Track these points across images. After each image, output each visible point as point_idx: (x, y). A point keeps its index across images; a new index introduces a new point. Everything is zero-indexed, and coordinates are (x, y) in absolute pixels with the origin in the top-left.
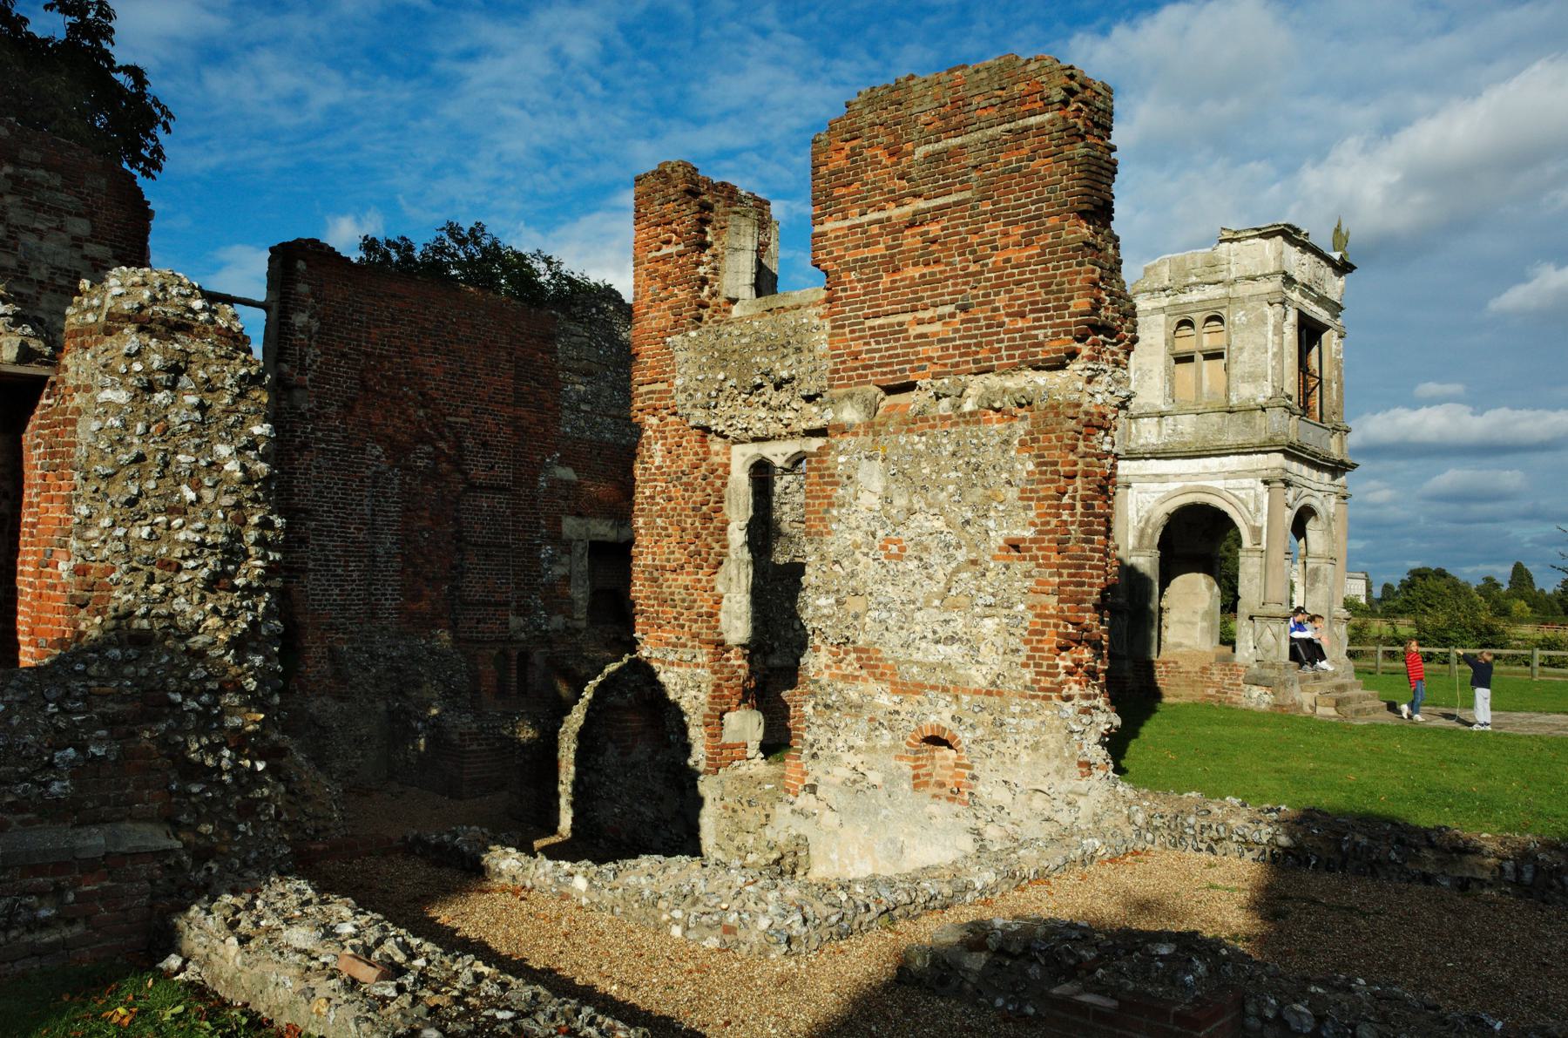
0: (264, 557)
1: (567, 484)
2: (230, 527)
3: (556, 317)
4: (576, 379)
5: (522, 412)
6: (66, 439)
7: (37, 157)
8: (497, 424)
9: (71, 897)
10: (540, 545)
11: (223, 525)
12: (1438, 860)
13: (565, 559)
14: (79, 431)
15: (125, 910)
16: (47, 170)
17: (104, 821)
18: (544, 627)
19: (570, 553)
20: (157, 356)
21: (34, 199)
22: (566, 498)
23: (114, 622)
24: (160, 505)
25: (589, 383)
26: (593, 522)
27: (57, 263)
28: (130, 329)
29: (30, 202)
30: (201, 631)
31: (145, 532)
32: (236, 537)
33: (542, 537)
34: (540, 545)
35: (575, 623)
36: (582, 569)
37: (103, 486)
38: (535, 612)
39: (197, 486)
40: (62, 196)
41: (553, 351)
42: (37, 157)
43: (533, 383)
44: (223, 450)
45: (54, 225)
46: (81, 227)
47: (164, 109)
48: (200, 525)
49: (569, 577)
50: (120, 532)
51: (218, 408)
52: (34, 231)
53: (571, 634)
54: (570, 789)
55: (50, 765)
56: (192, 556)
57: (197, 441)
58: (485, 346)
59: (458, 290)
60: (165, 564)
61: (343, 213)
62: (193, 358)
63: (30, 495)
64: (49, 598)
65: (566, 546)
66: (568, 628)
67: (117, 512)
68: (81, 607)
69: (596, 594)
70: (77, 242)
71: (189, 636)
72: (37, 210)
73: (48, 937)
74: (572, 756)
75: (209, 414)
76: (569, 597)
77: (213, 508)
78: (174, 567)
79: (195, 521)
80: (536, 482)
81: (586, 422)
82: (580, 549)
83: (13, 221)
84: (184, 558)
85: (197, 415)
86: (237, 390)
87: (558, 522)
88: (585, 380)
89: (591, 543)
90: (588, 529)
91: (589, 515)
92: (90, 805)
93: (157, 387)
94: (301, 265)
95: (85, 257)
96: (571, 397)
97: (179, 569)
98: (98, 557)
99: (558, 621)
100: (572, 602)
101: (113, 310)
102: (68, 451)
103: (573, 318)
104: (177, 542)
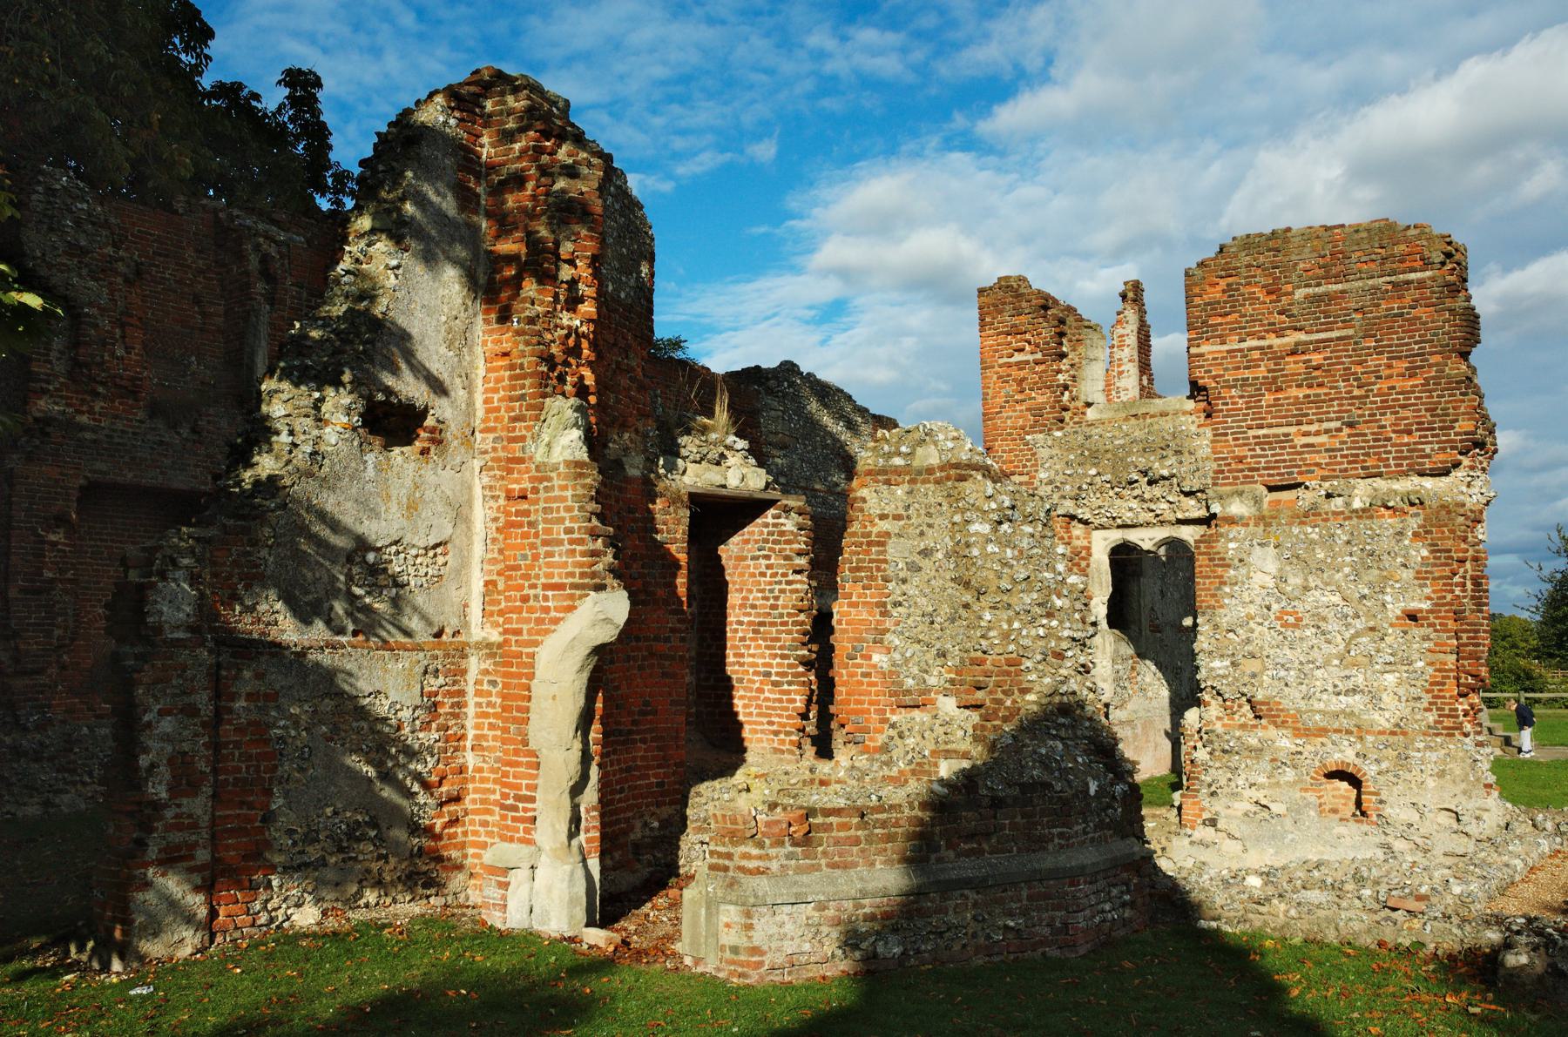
4: (775, 452)
6: (873, 557)
25: (785, 456)
88: (782, 453)
103: (770, 392)
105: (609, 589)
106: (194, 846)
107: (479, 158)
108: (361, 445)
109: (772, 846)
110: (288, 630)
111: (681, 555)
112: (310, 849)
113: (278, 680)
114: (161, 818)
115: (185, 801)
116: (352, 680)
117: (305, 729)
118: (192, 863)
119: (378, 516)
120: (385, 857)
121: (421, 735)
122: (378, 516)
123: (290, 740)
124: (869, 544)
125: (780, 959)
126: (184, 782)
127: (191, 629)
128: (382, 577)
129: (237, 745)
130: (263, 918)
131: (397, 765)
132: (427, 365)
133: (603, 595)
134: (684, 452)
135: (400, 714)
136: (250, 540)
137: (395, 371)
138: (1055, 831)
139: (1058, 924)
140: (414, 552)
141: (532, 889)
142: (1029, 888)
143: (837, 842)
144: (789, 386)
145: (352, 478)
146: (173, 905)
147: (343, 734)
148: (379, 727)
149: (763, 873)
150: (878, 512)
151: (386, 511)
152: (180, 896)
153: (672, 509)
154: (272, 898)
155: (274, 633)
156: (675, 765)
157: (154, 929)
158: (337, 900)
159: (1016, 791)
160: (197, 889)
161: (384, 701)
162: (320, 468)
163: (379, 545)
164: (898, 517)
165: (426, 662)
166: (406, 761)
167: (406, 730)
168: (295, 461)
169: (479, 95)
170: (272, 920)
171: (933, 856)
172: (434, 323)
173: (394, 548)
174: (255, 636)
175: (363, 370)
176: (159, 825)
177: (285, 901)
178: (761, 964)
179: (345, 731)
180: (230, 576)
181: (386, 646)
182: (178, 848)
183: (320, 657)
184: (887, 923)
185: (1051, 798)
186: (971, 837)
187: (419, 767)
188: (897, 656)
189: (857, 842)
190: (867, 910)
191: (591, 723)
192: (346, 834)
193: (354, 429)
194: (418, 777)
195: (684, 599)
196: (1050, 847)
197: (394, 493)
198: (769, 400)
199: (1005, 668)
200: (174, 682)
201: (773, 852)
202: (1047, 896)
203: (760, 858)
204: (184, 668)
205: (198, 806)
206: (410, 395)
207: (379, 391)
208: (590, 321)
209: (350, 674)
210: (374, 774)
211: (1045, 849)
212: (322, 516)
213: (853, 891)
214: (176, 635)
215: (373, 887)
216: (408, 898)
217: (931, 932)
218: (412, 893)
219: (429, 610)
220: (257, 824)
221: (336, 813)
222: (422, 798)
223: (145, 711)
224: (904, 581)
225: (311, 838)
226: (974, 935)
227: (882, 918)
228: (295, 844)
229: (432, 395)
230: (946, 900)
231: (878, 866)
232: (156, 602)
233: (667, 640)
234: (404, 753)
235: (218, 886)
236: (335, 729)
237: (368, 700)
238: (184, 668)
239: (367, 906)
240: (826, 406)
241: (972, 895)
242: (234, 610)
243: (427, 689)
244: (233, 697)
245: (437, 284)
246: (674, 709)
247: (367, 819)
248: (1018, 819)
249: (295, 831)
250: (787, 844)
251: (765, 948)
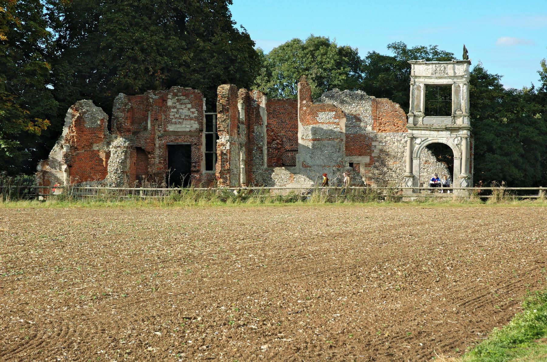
12: (42, 165)
42: (181, 94)
46: (189, 106)
61: (122, 136)
70: (189, 109)
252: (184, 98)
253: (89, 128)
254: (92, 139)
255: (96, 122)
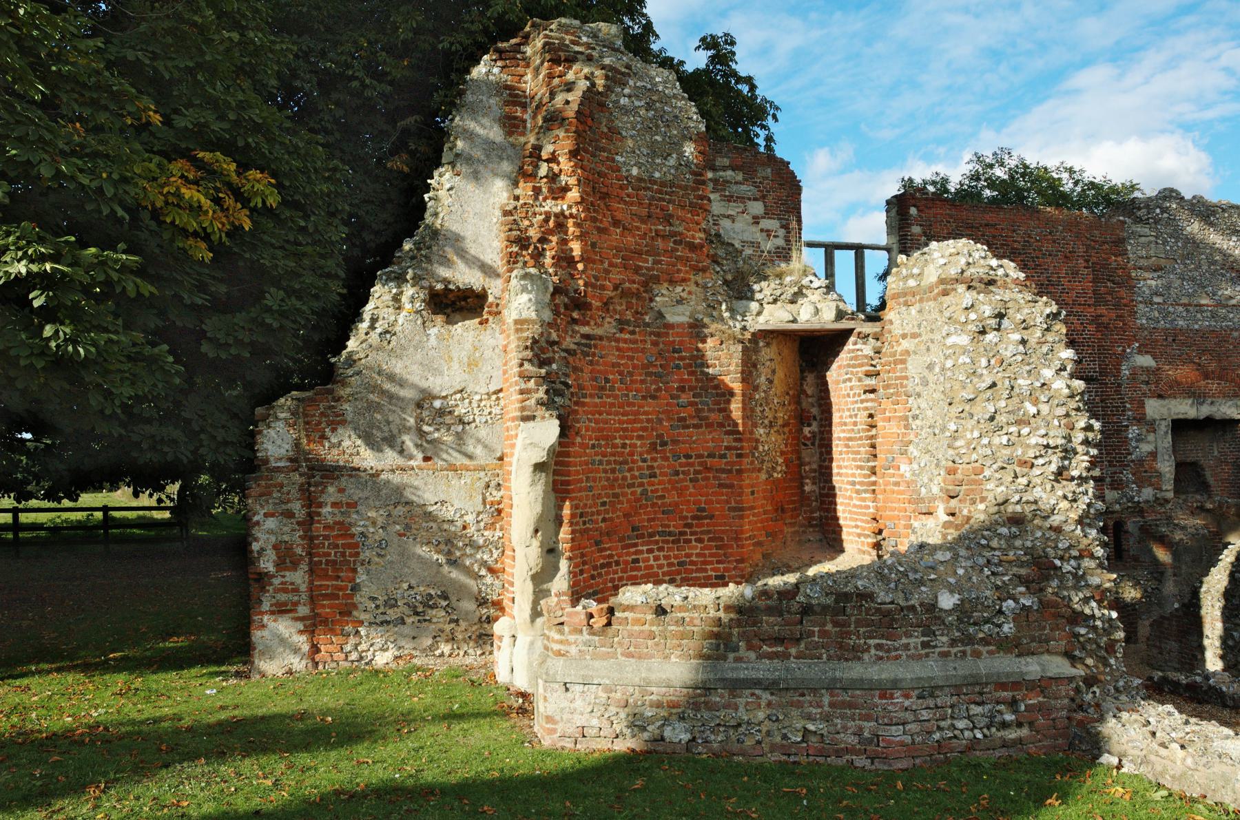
0: (1087, 453)
1: (1147, 370)
2: (1063, 431)
3: (1124, 222)
4: (1147, 275)
5: (1102, 310)
6: (898, 374)
7: (726, 162)
8: (1082, 324)
9: (1023, 708)
10: (1127, 426)
11: (1060, 431)
13: (1151, 437)
14: (910, 367)
15: (1054, 720)
16: (733, 170)
17: (1033, 654)
18: (1136, 499)
19: (1154, 431)
20: (986, 307)
21: (727, 193)
22: (1147, 383)
23: (997, 508)
24: (1012, 418)
25: (1159, 277)
26: (1173, 402)
27: (745, 239)
28: (961, 288)
29: (725, 196)
30: (1056, 512)
31: (1004, 440)
32: (1068, 438)
33: (1128, 419)
34: (1127, 426)
35: (1163, 494)
36: (1167, 445)
37: (967, 408)
38: (1127, 486)
39: (1036, 402)
40: (744, 187)
41: (1125, 252)
42: (726, 162)
43: (1109, 284)
44: (1048, 373)
45: (740, 210)
46: (757, 208)
47: (771, 103)
48: (1043, 432)
49: (1156, 453)
50: (985, 441)
51: (1033, 341)
52: (728, 217)
53: (1161, 505)
54: (1218, 643)
55: (1000, 612)
56: (1041, 456)
57: (1028, 368)
58: (1066, 257)
59: (1038, 211)
60: (1023, 463)
62: (1009, 305)
63: (841, 417)
64: (893, 492)
65: (1152, 426)
66: (1157, 499)
67: (982, 426)
68: (952, 497)
69: (1180, 466)
71: (1049, 517)
72: (729, 201)
73: (1012, 734)
74: (1218, 613)
75: (1028, 346)
76: (1157, 471)
77: (1049, 418)
78: (1030, 464)
79: (1037, 429)
80: (1119, 371)
81: (1160, 313)
82: (1164, 427)
83: (716, 212)
84: (1036, 457)
85: (1021, 348)
86: (1045, 326)
87: (1142, 405)
88: (1155, 275)
89: (1174, 421)
90: (1169, 409)
91: (1169, 396)
92: (1025, 641)
93: (987, 330)
94: (913, 211)
95: (762, 230)
96: (1144, 292)
97: (1032, 466)
98: (966, 459)
99: (1147, 493)
100: (1160, 475)
101: (943, 276)
102: (901, 384)
103: (1139, 220)
104: (1028, 446)
105: (538, 419)
106: (296, 604)
107: (525, 92)
108: (424, 323)
109: (570, 633)
110: (367, 459)
111: (737, 387)
112: (390, 612)
113: (356, 494)
114: (271, 584)
115: (287, 574)
116: (419, 493)
117: (382, 527)
118: (296, 615)
119: (441, 374)
120: (457, 621)
121: (486, 533)
122: (441, 374)
123: (370, 535)
124: (896, 363)
125: (571, 730)
126: (286, 559)
127: (291, 460)
128: (449, 417)
129: (326, 537)
130: (354, 656)
131: (464, 555)
132: (482, 257)
133: (531, 424)
134: (758, 296)
135: (466, 518)
136: (334, 398)
137: (447, 263)
138: (872, 642)
139: (866, 734)
140: (477, 397)
141: (512, 653)
142: (831, 695)
143: (631, 635)
144: (1162, 212)
145: (416, 348)
146: (283, 641)
147: (415, 532)
148: (446, 526)
149: (563, 655)
150: (901, 332)
151: (449, 368)
152: (287, 635)
153: (724, 346)
154: (360, 643)
155: (356, 462)
156: (737, 561)
157: (269, 654)
158: (414, 649)
159: (830, 601)
160: (301, 632)
161: (450, 508)
162: (389, 342)
163: (444, 394)
164: (914, 336)
165: (487, 480)
166: (472, 552)
167: (471, 530)
168: (370, 340)
169: (519, 45)
170: (361, 658)
171: (731, 656)
172: (487, 224)
173: (458, 396)
174: (341, 463)
175: (423, 269)
176: (271, 588)
177: (372, 645)
178: (554, 731)
179: (417, 529)
180: (319, 423)
181: (453, 468)
182: (285, 604)
183: (391, 477)
184: (674, 711)
185: (868, 610)
186: (780, 640)
187: (485, 557)
188: (915, 466)
189: (652, 636)
190: (654, 697)
191: (560, 524)
192: (421, 603)
193: (417, 312)
194: (484, 564)
195: (740, 421)
196: (866, 657)
197: (455, 355)
198: (1139, 229)
199: (973, 476)
200: (274, 495)
201: (572, 638)
202: (851, 706)
203: (561, 642)
204: (282, 486)
205: (298, 577)
206: (467, 281)
207: (437, 282)
208: (577, 203)
209: (416, 488)
210: (444, 561)
211: (859, 659)
212: (391, 378)
213: (637, 679)
214: (279, 464)
215: (447, 641)
216: (479, 652)
217: (719, 725)
218: (482, 648)
219: (492, 441)
220: (349, 592)
221: (410, 587)
222: (489, 579)
223: (254, 514)
224: (919, 395)
225: (391, 603)
226: (768, 733)
227: (669, 706)
228: (377, 607)
229: (487, 279)
230: (734, 697)
231: (673, 659)
232: (263, 443)
233: (723, 456)
234: (471, 546)
235: (317, 632)
236: (408, 527)
237: (435, 507)
238: (282, 486)
239: (442, 655)
240: (1211, 224)
241: (766, 696)
242: (324, 447)
243: (489, 499)
244: (320, 505)
245: (487, 196)
246: (732, 514)
247: (439, 593)
248: (829, 627)
249: (376, 598)
250: (585, 633)
251: (557, 718)
252: (740, 177)
253: (640, 179)
254: (652, 252)
255: (676, 146)
